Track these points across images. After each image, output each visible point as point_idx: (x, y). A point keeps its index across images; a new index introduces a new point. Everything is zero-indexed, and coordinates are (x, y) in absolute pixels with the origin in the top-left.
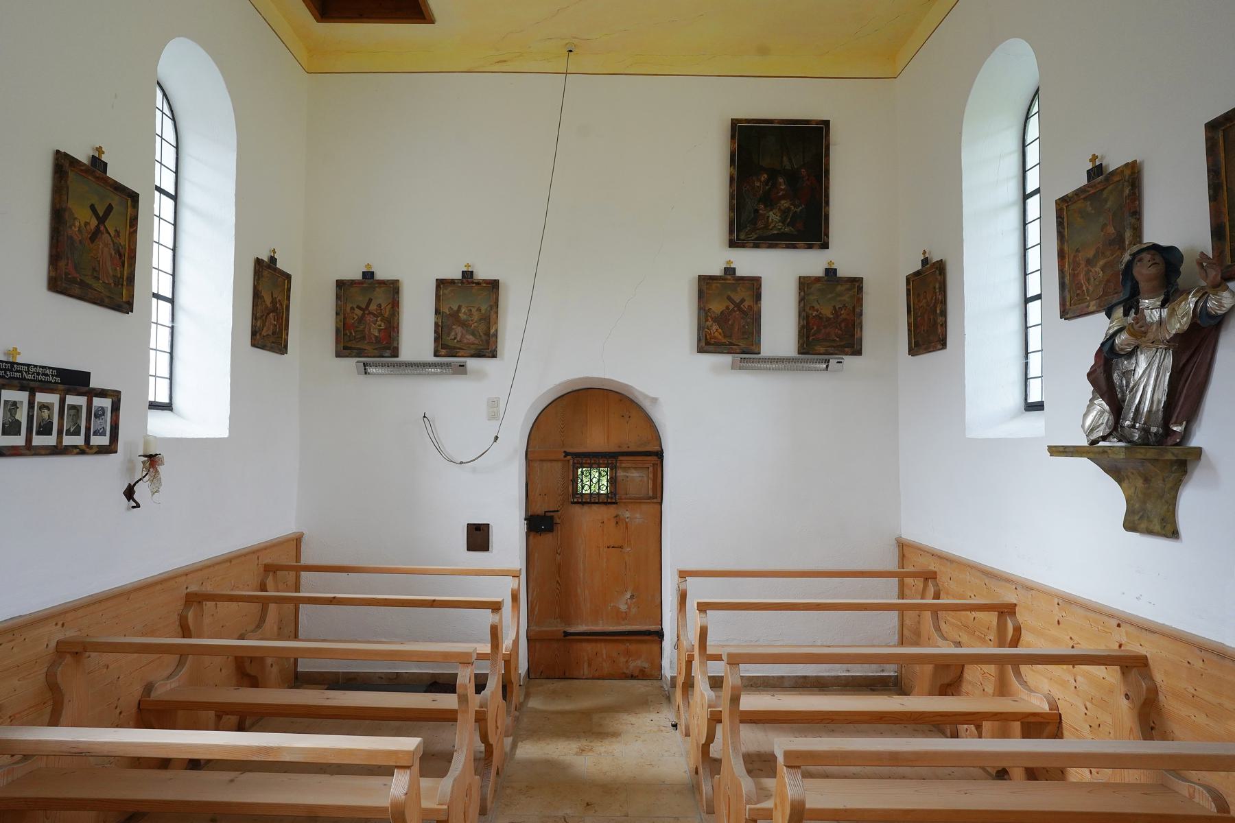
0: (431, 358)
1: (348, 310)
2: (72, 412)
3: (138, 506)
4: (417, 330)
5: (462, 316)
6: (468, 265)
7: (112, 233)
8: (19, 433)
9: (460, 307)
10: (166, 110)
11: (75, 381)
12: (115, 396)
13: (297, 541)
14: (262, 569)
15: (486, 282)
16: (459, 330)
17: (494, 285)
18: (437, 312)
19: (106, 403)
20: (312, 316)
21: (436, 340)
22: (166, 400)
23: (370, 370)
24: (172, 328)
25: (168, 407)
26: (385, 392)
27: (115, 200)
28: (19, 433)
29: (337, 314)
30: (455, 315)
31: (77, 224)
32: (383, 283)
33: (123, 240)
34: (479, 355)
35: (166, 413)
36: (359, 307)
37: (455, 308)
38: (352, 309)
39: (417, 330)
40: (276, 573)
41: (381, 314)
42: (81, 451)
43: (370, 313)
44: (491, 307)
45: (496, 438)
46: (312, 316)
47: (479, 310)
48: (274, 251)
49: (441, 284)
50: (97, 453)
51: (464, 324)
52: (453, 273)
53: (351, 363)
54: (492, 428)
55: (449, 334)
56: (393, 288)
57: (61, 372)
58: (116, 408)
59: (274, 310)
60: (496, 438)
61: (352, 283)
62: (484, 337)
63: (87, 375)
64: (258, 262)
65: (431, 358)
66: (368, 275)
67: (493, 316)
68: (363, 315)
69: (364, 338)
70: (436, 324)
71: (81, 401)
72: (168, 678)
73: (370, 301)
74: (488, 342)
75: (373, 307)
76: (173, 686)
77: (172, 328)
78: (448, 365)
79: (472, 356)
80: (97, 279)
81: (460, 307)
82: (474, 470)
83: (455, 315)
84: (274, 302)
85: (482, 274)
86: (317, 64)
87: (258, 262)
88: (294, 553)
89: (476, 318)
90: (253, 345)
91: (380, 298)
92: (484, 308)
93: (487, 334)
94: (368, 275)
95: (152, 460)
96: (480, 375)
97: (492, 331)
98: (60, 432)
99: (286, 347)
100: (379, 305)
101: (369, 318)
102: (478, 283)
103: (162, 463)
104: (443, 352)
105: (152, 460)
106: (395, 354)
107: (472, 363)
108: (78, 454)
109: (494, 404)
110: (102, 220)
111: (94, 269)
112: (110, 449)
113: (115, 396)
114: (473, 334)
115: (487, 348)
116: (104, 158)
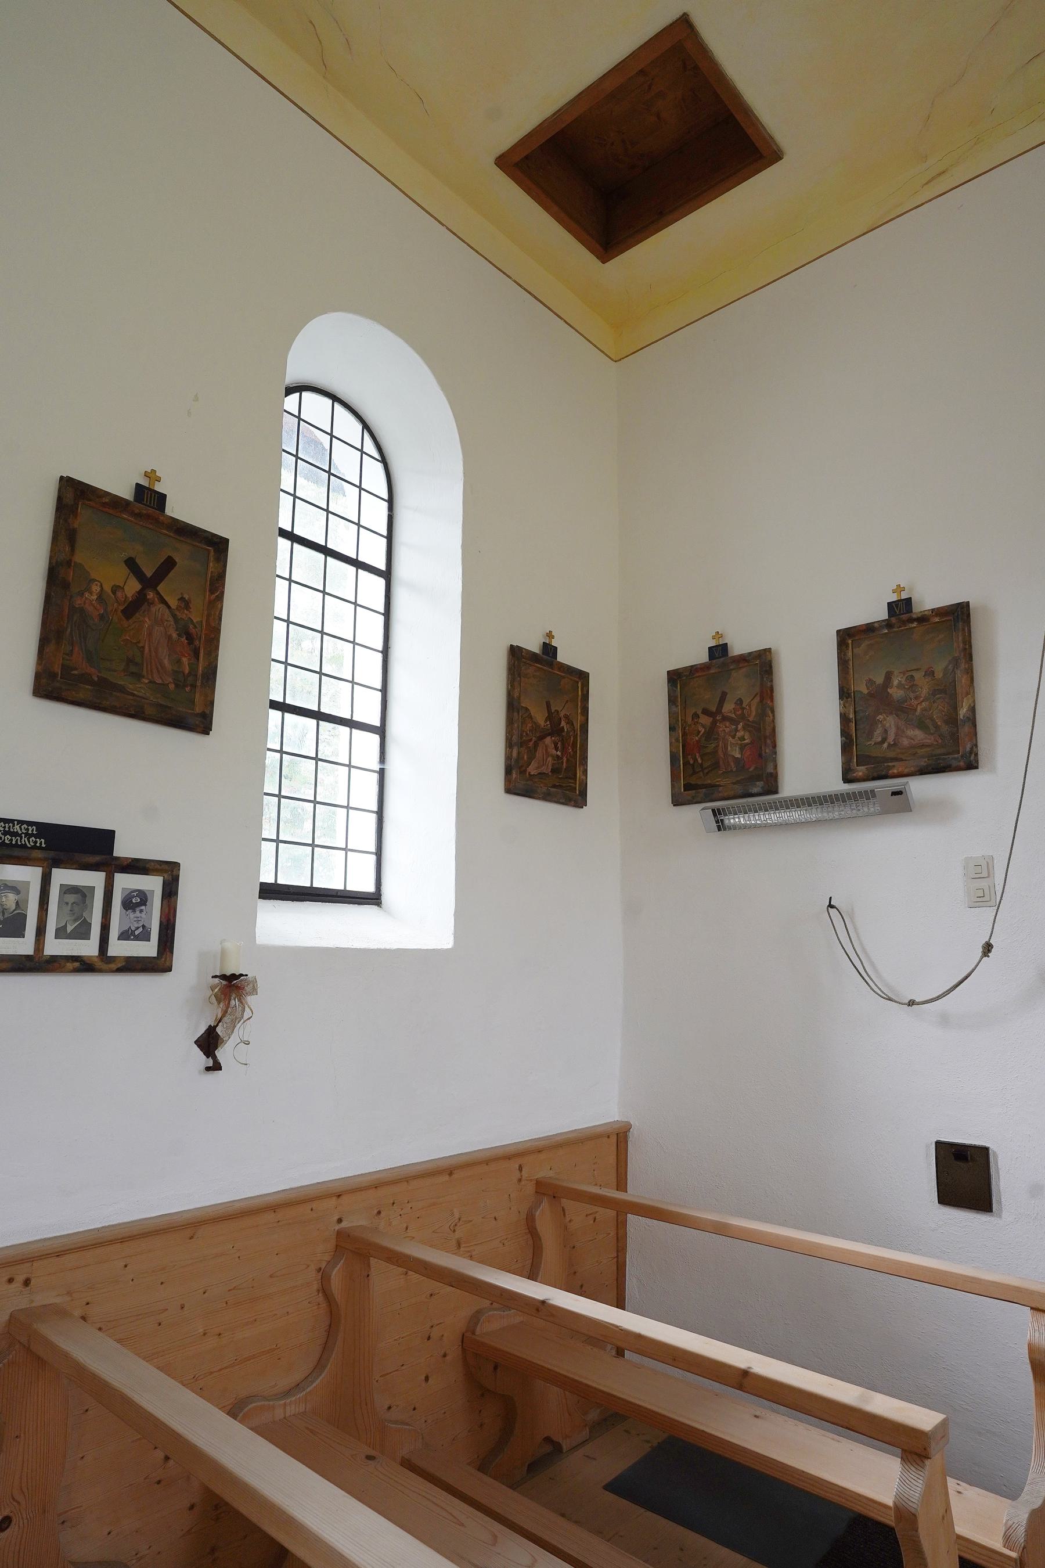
0: (838, 786)
1: (689, 720)
2: (71, 898)
3: (216, 1067)
4: (809, 739)
5: (896, 693)
6: (899, 589)
7: (173, 603)
8: (148, 939)
9: (888, 677)
10: (370, 447)
11: (90, 847)
12: (170, 874)
13: (618, 1138)
14: (530, 1189)
15: (940, 612)
16: (890, 722)
17: (958, 617)
18: (844, 693)
19: (153, 884)
20: (626, 737)
21: (846, 748)
22: (370, 888)
23: (731, 820)
24: (382, 773)
25: (374, 899)
26: (766, 867)
27: (182, 554)
28: (148, 939)
29: (672, 729)
30: (880, 695)
31: (96, 588)
32: (744, 659)
33: (196, 615)
34: (937, 767)
35: (367, 911)
36: (706, 712)
37: (879, 680)
38: (696, 716)
39: (809, 739)
40: (573, 1199)
41: (743, 717)
42: (83, 966)
43: (725, 718)
44: (956, 662)
45: (988, 948)
46: (626, 737)
47: (930, 673)
48: (550, 635)
49: (846, 638)
50: (120, 970)
51: (900, 709)
52: (872, 610)
53: (696, 815)
54: (976, 926)
55: (870, 735)
56: (762, 665)
57: (45, 830)
58: (170, 892)
59: (555, 730)
60: (988, 948)
61: (693, 670)
62: (945, 729)
63: (110, 835)
64: (515, 653)
65: (838, 786)
66: (719, 651)
67: (962, 680)
68: (714, 723)
69: (716, 765)
70: (844, 719)
71: (95, 879)
72: (288, 1393)
73: (723, 697)
74: (955, 738)
75: (728, 707)
76: (291, 1410)
77: (382, 773)
78: (870, 795)
79: (923, 772)
80: (138, 676)
81: (888, 677)
82: (945, 1020)
83: (880, 695)
84: (551, 716)
85: (930, 598)
86: (625, 335)
87: (515, 653)
88: (612, 1159)
89: (924, 692)
90: (509, 790)
91: (741, 687)
92: (939, 669)
93: (952, 720)
94: (719, 651)
95: (231, 986)
96: (942, 811)
97: (963, 712)
98: (41, 931)
99: (583, 794)
100: (740, 702)
101: (723, 728)
102: (923, 619)
103: (254, 991)
104: (861, 771)
105: (231, 986)
106: (771, 786)
107: (920, 787)
108: (76, 971)
109: (980, 871)
110: (150, 583)
111: (130, 661)
112: (160, 964)
113: (170, 874)
114: (921, 725)
115: (955, 750)
116: (159, 488)
